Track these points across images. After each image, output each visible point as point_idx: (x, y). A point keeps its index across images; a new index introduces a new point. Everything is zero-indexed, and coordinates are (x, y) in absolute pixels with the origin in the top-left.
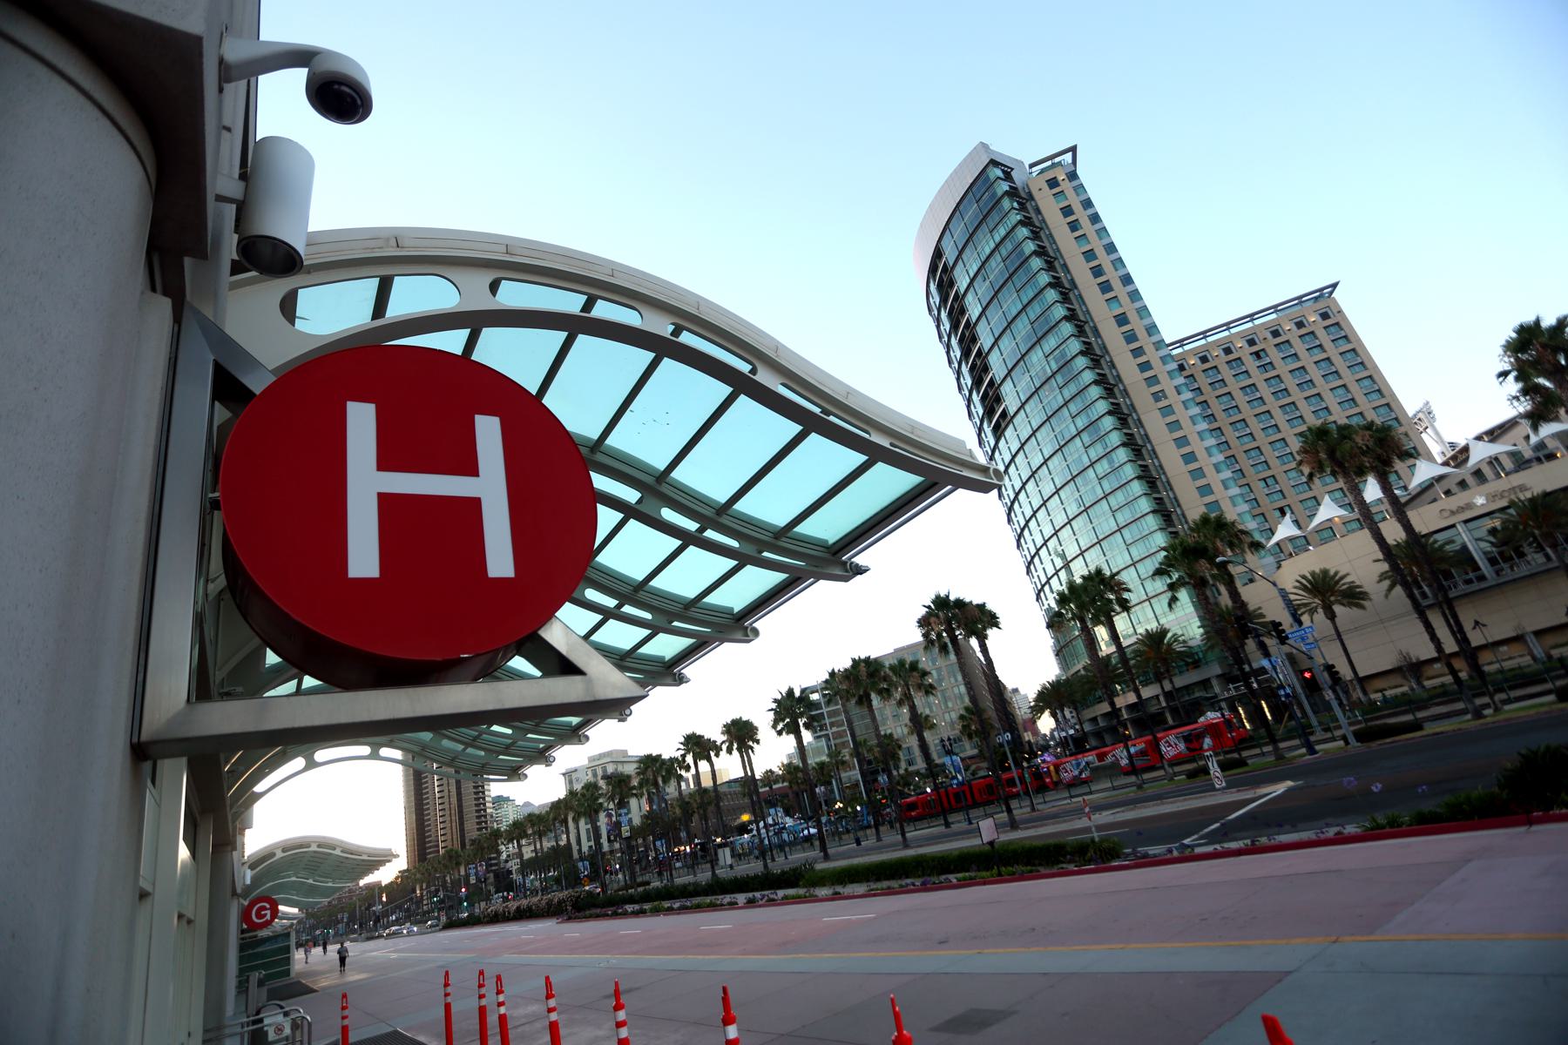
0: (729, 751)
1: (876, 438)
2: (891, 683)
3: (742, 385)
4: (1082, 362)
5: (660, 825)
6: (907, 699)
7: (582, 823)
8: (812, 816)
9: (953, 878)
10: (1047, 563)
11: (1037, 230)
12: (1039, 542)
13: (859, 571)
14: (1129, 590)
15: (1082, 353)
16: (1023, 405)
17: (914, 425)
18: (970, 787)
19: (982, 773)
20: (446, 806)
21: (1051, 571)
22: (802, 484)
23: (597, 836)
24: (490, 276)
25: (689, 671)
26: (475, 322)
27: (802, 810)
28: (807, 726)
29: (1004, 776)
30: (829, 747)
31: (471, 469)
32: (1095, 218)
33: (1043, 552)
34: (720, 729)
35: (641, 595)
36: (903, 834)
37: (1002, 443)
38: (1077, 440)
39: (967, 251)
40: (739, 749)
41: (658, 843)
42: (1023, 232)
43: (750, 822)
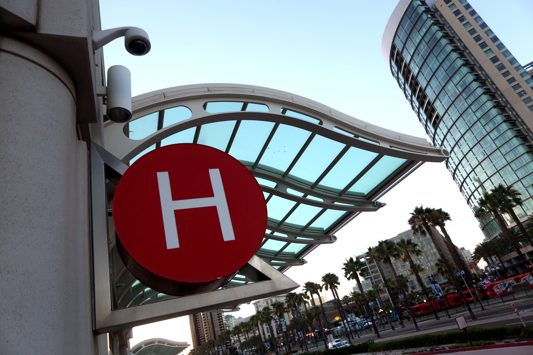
0: (327, 289)
1: (383, 145)
2: (399, 252)
3: (316, 130)
4: (475, 85)
5: (299, 324)
6: (408, 258)
7: (264, 325)
8: (369, 315)
9: (446, 347)
10: (470, 185)
11: (442, 24)
12: (465, 175)
13: (381, 205)
14: (520, 194)
15: (475, 80)
16: (446, 111)
17: (400, 135)
18: (447, 299)
19: (451, 291)
20: (206, 321)
21: (473, 189)
22: (350, 169)
23: (272, 331)
24: (202, 102)
25: (306, 258)
26: (197, 123)
27: (363, 313)
28: (361, 275)
29: (464, 292)
30: (372, 283)
31: (210, 194)
32: (473, 13)
33: (468, 180)
34: (321, 279)
35: (282, 227)
36: (416, 324)
37: (438, 131)
38: (478, 123)
39: (408, 43)
40: (331, 288)
41: (299, 333)
42: (436, 28)
43: (340, 321)
